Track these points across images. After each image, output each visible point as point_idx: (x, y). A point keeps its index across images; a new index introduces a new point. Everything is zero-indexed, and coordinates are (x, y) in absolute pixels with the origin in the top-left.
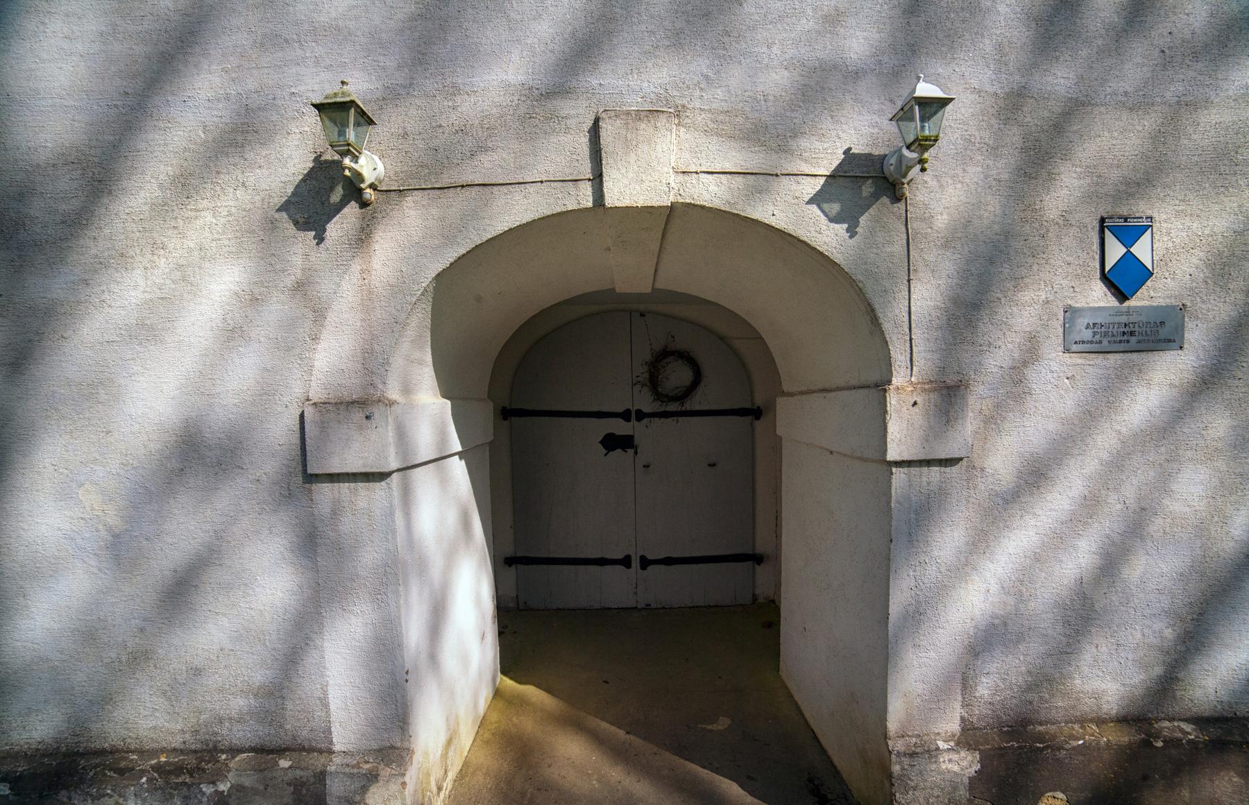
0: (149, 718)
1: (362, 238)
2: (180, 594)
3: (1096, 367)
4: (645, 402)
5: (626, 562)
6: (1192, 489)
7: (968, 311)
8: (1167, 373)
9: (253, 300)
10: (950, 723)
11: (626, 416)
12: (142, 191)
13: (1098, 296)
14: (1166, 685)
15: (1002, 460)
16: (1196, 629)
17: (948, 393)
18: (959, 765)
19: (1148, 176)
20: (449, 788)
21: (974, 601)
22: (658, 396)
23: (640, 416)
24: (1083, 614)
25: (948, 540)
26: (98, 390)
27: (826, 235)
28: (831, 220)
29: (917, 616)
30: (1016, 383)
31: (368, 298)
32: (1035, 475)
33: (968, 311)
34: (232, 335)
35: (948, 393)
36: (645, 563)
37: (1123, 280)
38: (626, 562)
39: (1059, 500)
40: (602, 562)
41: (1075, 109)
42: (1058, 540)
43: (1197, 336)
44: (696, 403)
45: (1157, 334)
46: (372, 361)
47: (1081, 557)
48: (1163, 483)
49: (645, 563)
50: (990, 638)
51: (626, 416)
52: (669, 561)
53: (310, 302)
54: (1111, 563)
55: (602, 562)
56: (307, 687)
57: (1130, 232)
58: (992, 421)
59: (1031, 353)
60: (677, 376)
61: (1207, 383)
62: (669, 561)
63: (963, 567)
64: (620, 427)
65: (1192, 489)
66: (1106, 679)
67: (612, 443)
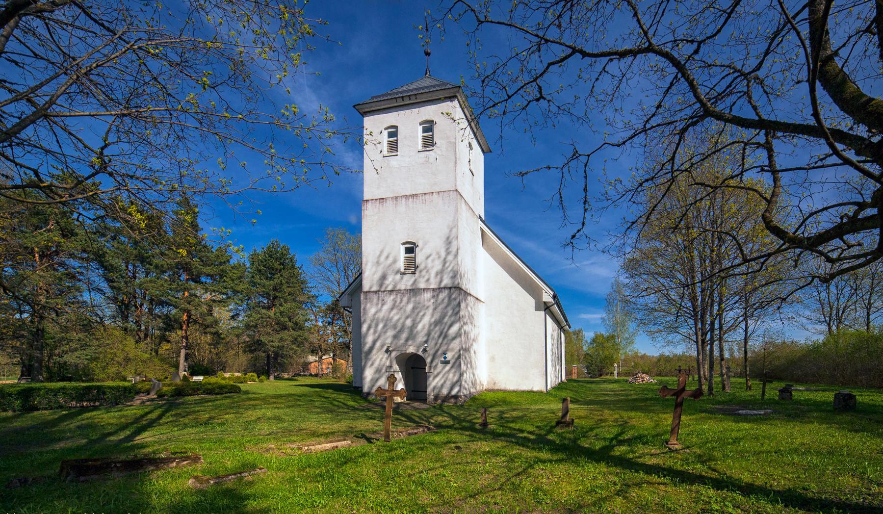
6: (451, 375)
8: (448, 367)
12: (374, 351)
14: (450, 393)
15: (436, 373)
16: (452, 389)
17: (430, 367)
20: (818, 399)
25: (431, 379)
28: (763, 216)
32: (438, 374)
35: (430, 367)
37: (445, 358)
39: (440, 376)
43: (452, 363)
47: (442, 381)
50: (434, 388)
54: (445, 382)
61: (452, 367)
65: (451, 375)
66: (445, 391)
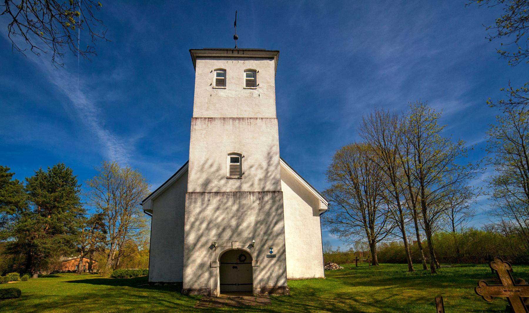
0: (196, 286)
1: (215, 250)
2: (199, 277)
3: (269, 259)
4: (239, 262)
5: (236, 284)
7: (258, 256)
9: (207, 254)
10: (259, 286)
11: (236, 264)
13: (269, 254)
15: (262, 266)
16: (278, 281)
17: (257, 261)
18: (259, 290)
19: (272, 245)
21: (259, 277)
22: (240, 261)
23: (238, 264)
24: (269, 278)
25: (257, 273)
26: (194, 261)
27: (248, 250)
29: (256, 278)
30: (263, 260)
31: (216, 255)
32: (265, 267)
33: (258, 256)
34: (205, 257)
35: (257, 261)
36: (238, 285)
38: (236, 284)
39: (267, 269)
40: (232, 284)
41: (267, 240)
42: (267, 273)
43: (277, 256)
44: (245, 262)
45: (274, 256)
46: (216, 259)
47: (268, 274)
48: (275, 268)
49: (238, 285)
50: (261, 280)
51: (236, 264)
52: (242, 284)
53: (211, 254)
54: (271, 274)
55: (232, 284)
56: (209, 284)
57: (271, 249)
58: (261, 263)
59: (264, 258)
60: (243, 258)
61: (278, 260)
62: (242, 284)
63: (259, 274)
64: (235, 265)
66: (271, 284)
67: (234, 267)
